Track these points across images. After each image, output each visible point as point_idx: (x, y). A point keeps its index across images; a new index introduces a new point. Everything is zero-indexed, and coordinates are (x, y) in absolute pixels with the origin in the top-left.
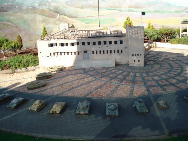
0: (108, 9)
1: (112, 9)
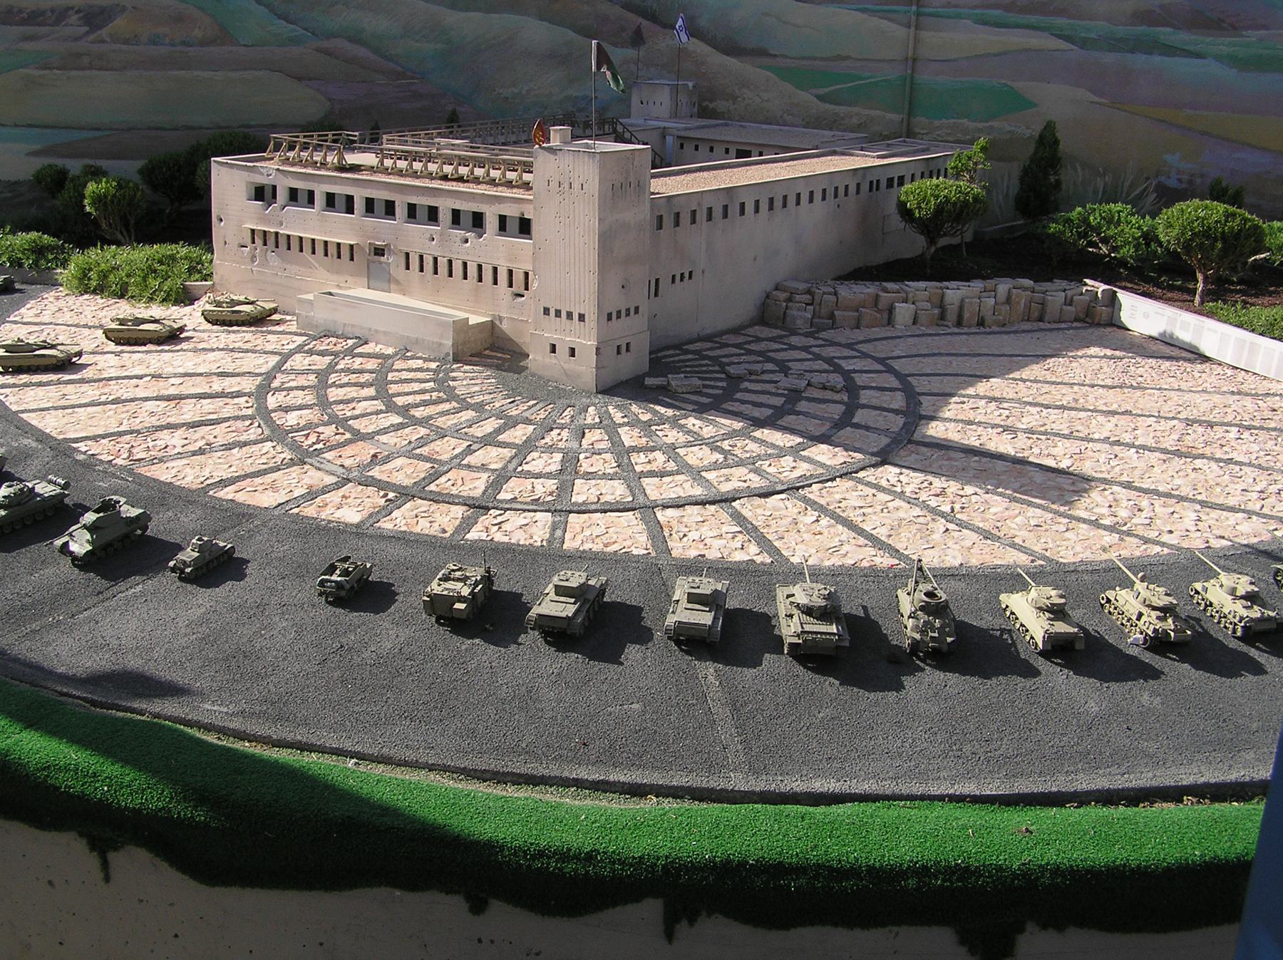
0: (984, 23)
1: (1017, 26)
